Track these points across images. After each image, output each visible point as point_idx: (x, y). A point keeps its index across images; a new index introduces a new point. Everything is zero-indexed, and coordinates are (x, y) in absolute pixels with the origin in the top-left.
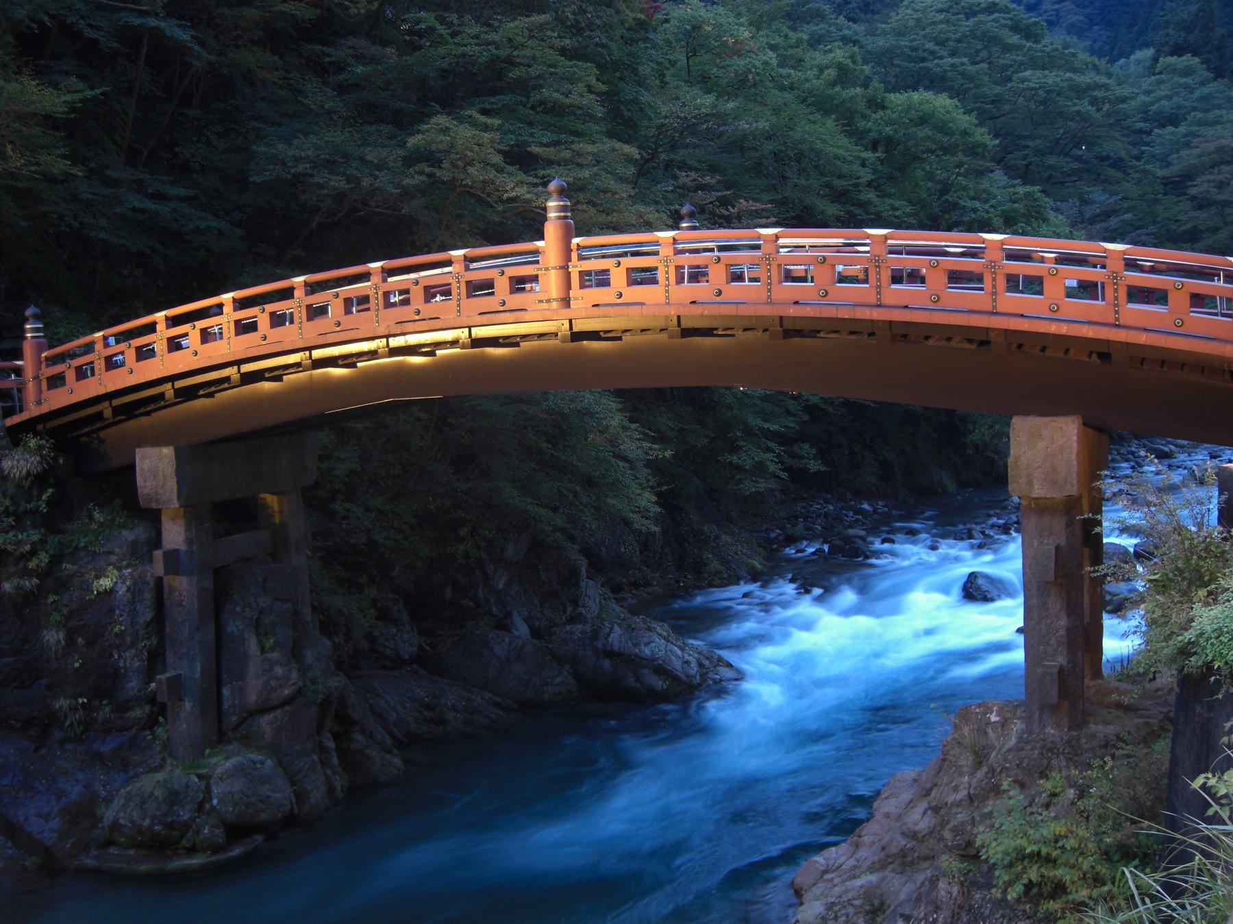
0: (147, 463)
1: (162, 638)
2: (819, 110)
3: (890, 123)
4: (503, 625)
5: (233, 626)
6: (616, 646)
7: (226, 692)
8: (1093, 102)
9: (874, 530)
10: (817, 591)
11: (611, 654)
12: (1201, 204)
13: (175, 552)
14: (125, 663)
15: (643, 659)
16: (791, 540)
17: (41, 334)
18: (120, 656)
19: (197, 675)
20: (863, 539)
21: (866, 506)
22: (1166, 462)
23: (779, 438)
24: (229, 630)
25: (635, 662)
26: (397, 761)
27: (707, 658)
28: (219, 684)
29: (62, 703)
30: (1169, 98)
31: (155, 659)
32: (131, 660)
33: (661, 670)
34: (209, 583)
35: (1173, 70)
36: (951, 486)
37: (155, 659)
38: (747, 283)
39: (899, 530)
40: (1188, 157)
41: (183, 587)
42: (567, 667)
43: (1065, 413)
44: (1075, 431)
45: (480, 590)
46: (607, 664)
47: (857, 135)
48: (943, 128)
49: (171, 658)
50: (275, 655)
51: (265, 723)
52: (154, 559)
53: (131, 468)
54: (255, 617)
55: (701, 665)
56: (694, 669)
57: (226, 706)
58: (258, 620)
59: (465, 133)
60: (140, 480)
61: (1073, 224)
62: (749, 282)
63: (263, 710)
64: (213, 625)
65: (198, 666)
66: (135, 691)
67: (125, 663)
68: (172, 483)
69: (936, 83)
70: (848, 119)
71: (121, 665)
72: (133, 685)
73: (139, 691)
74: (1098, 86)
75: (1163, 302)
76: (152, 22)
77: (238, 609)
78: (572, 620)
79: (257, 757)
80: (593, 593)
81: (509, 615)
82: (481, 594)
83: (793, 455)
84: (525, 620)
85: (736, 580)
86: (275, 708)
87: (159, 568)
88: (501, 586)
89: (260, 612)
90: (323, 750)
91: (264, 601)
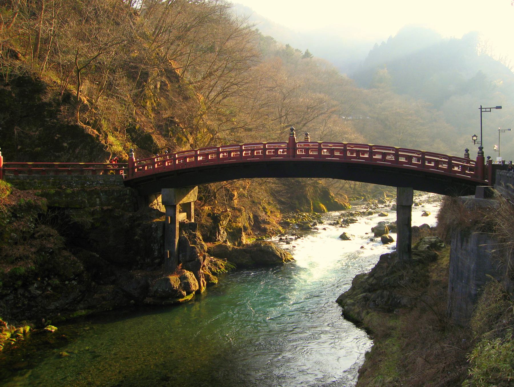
7: (181, 256)
18: (153, 245)
32: (156, 247)
57: (180, 259)
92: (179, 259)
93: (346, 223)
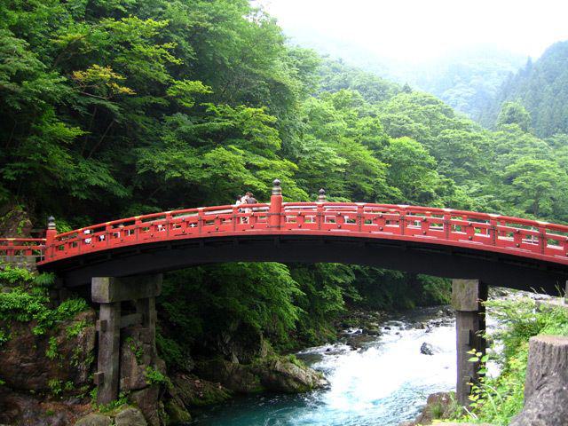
0: (96, 284)
2: (165, 64)
3: (392, 152)
4: (229, 358)
5: (127, 353)
6: (278, 368)
7: (122, 381)
8: (475, 144)
9: (381, 323)
10: (359, 349)
11: (277, 372)
12: (519, 188)
13: (106, 321)
16: (346, 327)
17: (561, 248)
20: (377, 327)
21: (377, 313)
22: (504, 297)
23: (343, 285)
25: (286, 376)
26: (188, 414)
28: (119, 378)
29: (52, 383)
30: (505, 141)
31: (93, 367)
33: (297, 380)
34: (118, 335)
35: (507, 130)
36: (413, 306)
39: (392, 324)
40: (512, 168)
41: (110, 337)
43: (474, 278)
46: (274, 376)
47: (378, 156)
48: (412, 154)
51: (137, 395)
55: (313, 378)
56: (310, 380)
57: (121, 387)
59: (228, 155)
60: (93, 291)
63: (137, 390)
65: (112, 369)
68: (107, 293)
69: (408, 134)
70: (373, 147)
72: (83, 376)
74: (477, 138)
76: (104, 103)
78: (257, 356)
79: (134, 409)
80: (266, 345)
81: (231, 354)
83: (348, 291)
85: (322, 343)
86: (142, 389)
87: (99, 328)
90: (160, 409)
91: (139, 343)
92: (467, 312)
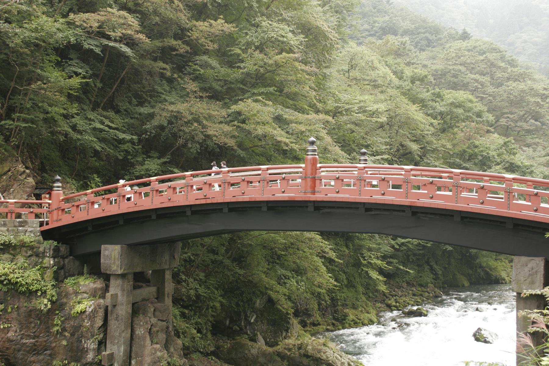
0: (107, 253)
1: (105, 334)
14: (87, 345)
15: (322, 360)
18: (85, 342)
19: (122, 354)
24: (137, 333)
27: (352, 362)
31: (102, 344)
32: (91, 345)
37: (102, 344)
38: (391, 189)
42: (286, 361)
44: (543, 264)
45: (243, 322)
49: (108, 345)
50: (158, 346)
52: (106, 298)
53: (99, 253)
54: (149, 328)
58: (150, 329)
60: (102, 261)
61: (522, 100)
62: (392, 188)
64: (130, 330)
65: (122, 349)
66: (91, 359)
67: (87, 345)
71: (85, 346)
73: (92, 359)
75: (535, 345)
77: (141, 323)
82: (243, 324)
84: (264, 338)
88: (252, 321)
89: (151, 326)
91: (154, 320)
93: (85, 348)
